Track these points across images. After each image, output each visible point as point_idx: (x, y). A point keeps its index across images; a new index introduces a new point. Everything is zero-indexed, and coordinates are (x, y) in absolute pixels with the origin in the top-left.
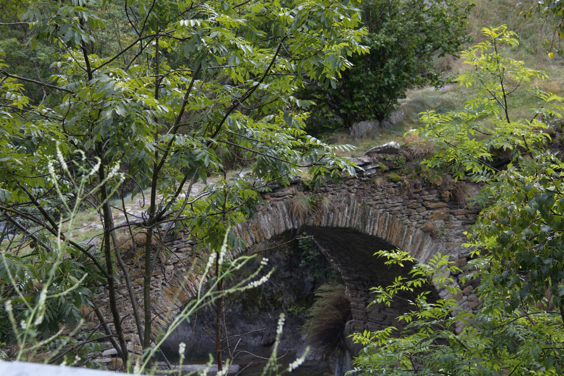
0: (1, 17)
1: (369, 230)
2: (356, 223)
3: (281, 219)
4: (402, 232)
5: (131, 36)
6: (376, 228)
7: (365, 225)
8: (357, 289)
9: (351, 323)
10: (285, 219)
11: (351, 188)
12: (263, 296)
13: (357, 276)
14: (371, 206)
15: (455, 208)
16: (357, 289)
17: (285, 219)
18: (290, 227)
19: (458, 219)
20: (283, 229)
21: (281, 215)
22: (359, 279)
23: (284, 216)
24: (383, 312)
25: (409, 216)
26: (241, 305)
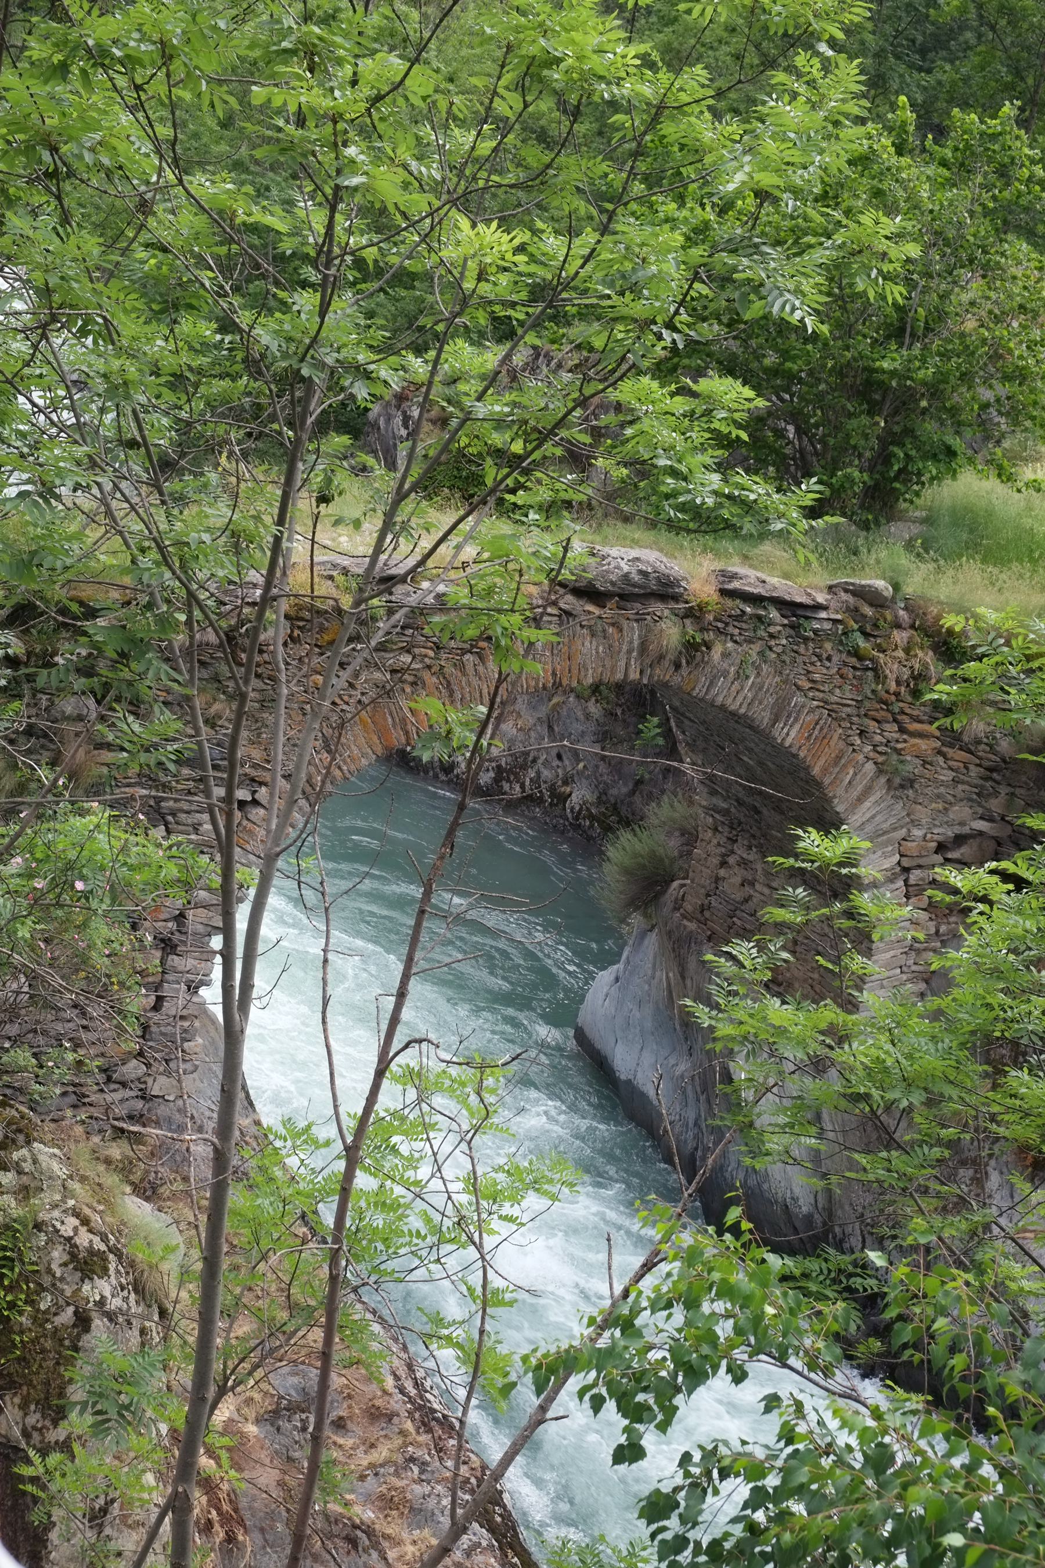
0: (1, 270)
1: (779, 732)
2: (763, 716)
3: (623, 656)
4: (839, 758)
5: (732, 1021)
6: (793, 734)
7: (776, 720)
8: (716, 830)
9: (683, 886)
10: (629, 659)
11: (772, 643)
12: (538, 773)
13: (725, 805)
14: (799, 688)
15: (952, 746)
16: (716, 830)
17: (629, 659)
18: (634, 675)
19: (951, 768)
20: (619, 676)
21: (625, 648)
22: (726, 812)
23: (629, 652)
24: (747, 888)
25: (862, 733)
26: (492, 774)
